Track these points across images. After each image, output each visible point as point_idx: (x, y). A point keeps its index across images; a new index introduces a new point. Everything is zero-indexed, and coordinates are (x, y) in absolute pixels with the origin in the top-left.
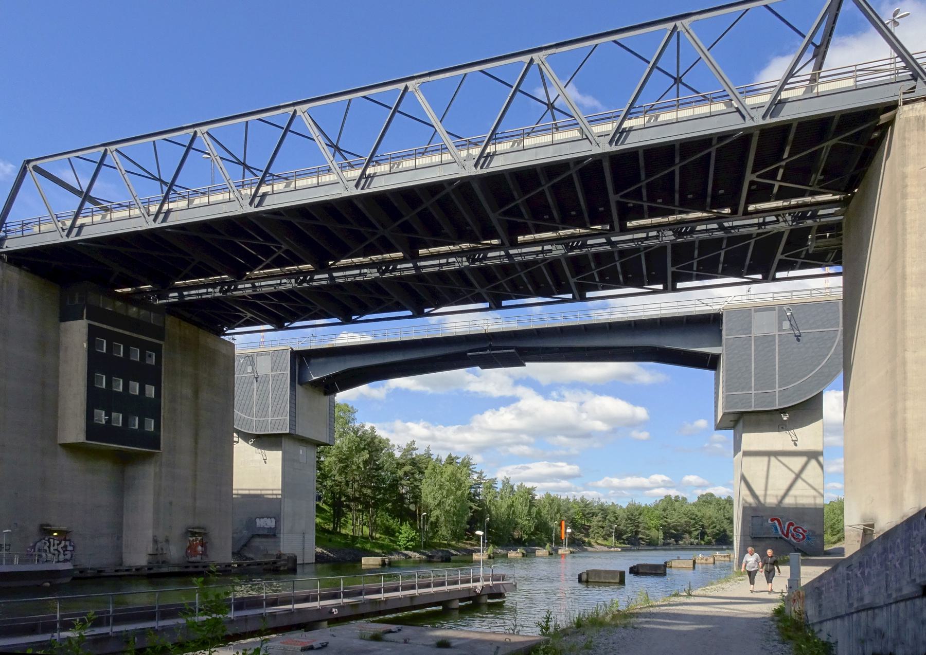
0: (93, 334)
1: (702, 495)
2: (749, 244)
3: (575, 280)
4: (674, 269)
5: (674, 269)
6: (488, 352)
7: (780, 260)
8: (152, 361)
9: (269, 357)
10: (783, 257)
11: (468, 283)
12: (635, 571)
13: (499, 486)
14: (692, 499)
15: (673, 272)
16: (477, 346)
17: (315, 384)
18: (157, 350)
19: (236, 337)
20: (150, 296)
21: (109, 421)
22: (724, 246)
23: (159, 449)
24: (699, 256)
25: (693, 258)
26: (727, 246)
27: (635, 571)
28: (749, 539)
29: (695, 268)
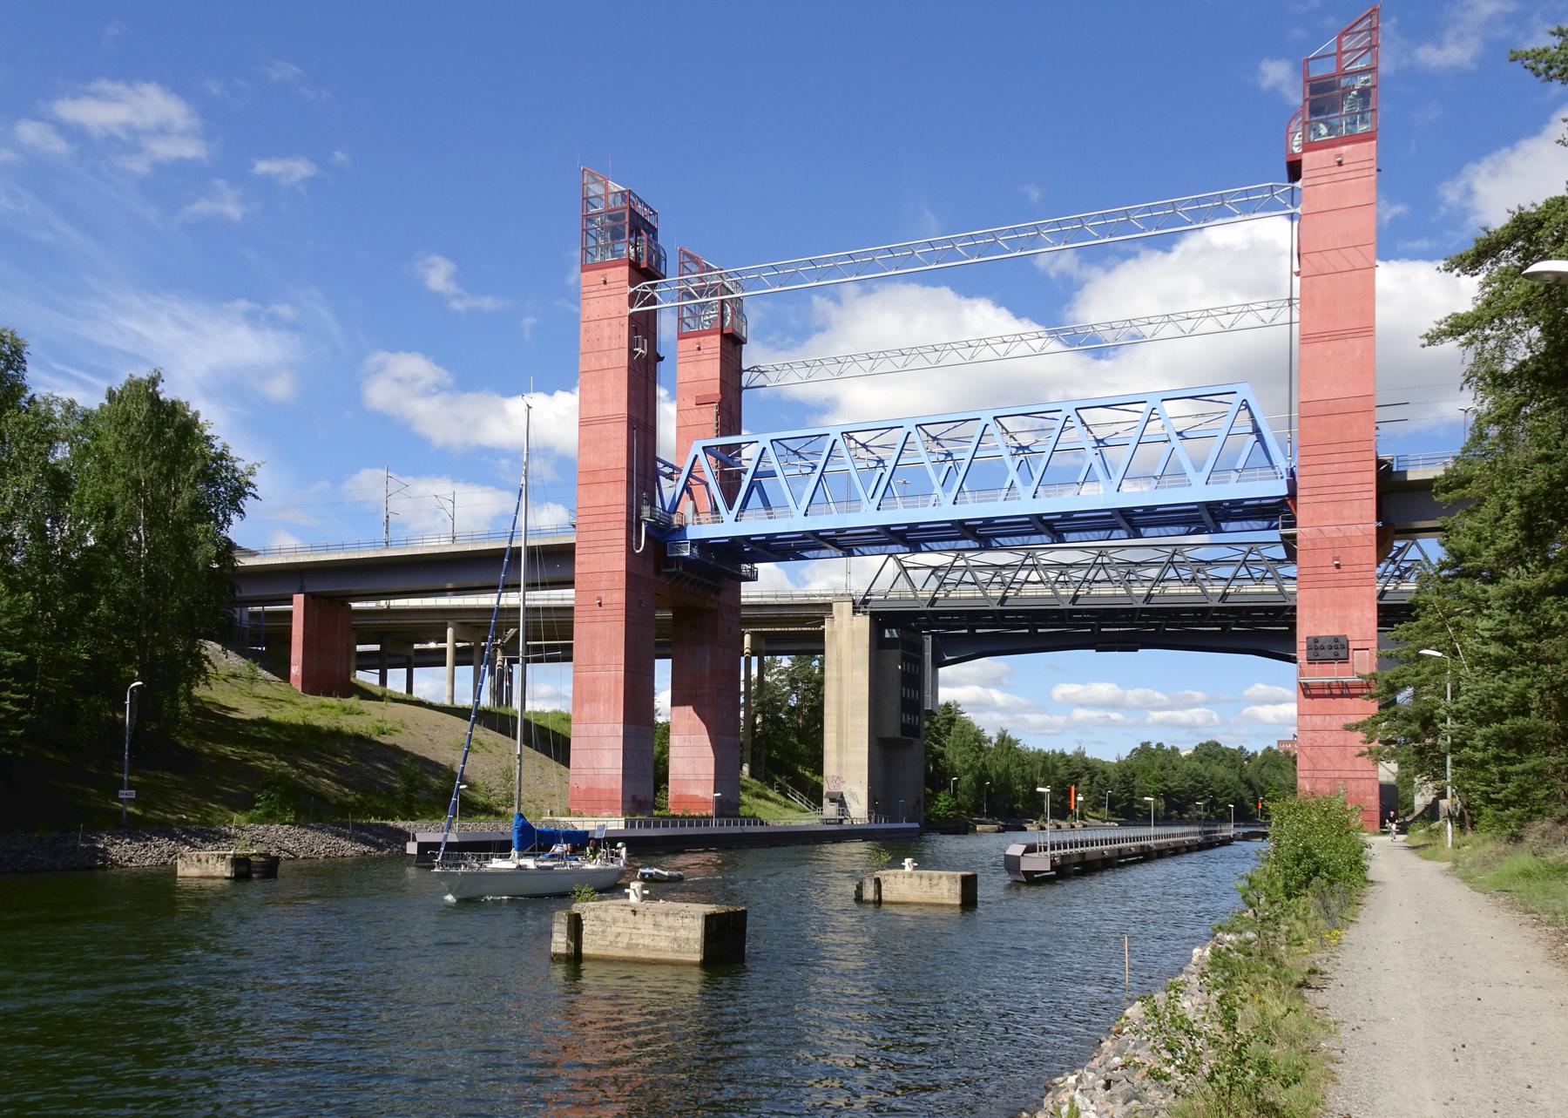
14: (1186, 751)
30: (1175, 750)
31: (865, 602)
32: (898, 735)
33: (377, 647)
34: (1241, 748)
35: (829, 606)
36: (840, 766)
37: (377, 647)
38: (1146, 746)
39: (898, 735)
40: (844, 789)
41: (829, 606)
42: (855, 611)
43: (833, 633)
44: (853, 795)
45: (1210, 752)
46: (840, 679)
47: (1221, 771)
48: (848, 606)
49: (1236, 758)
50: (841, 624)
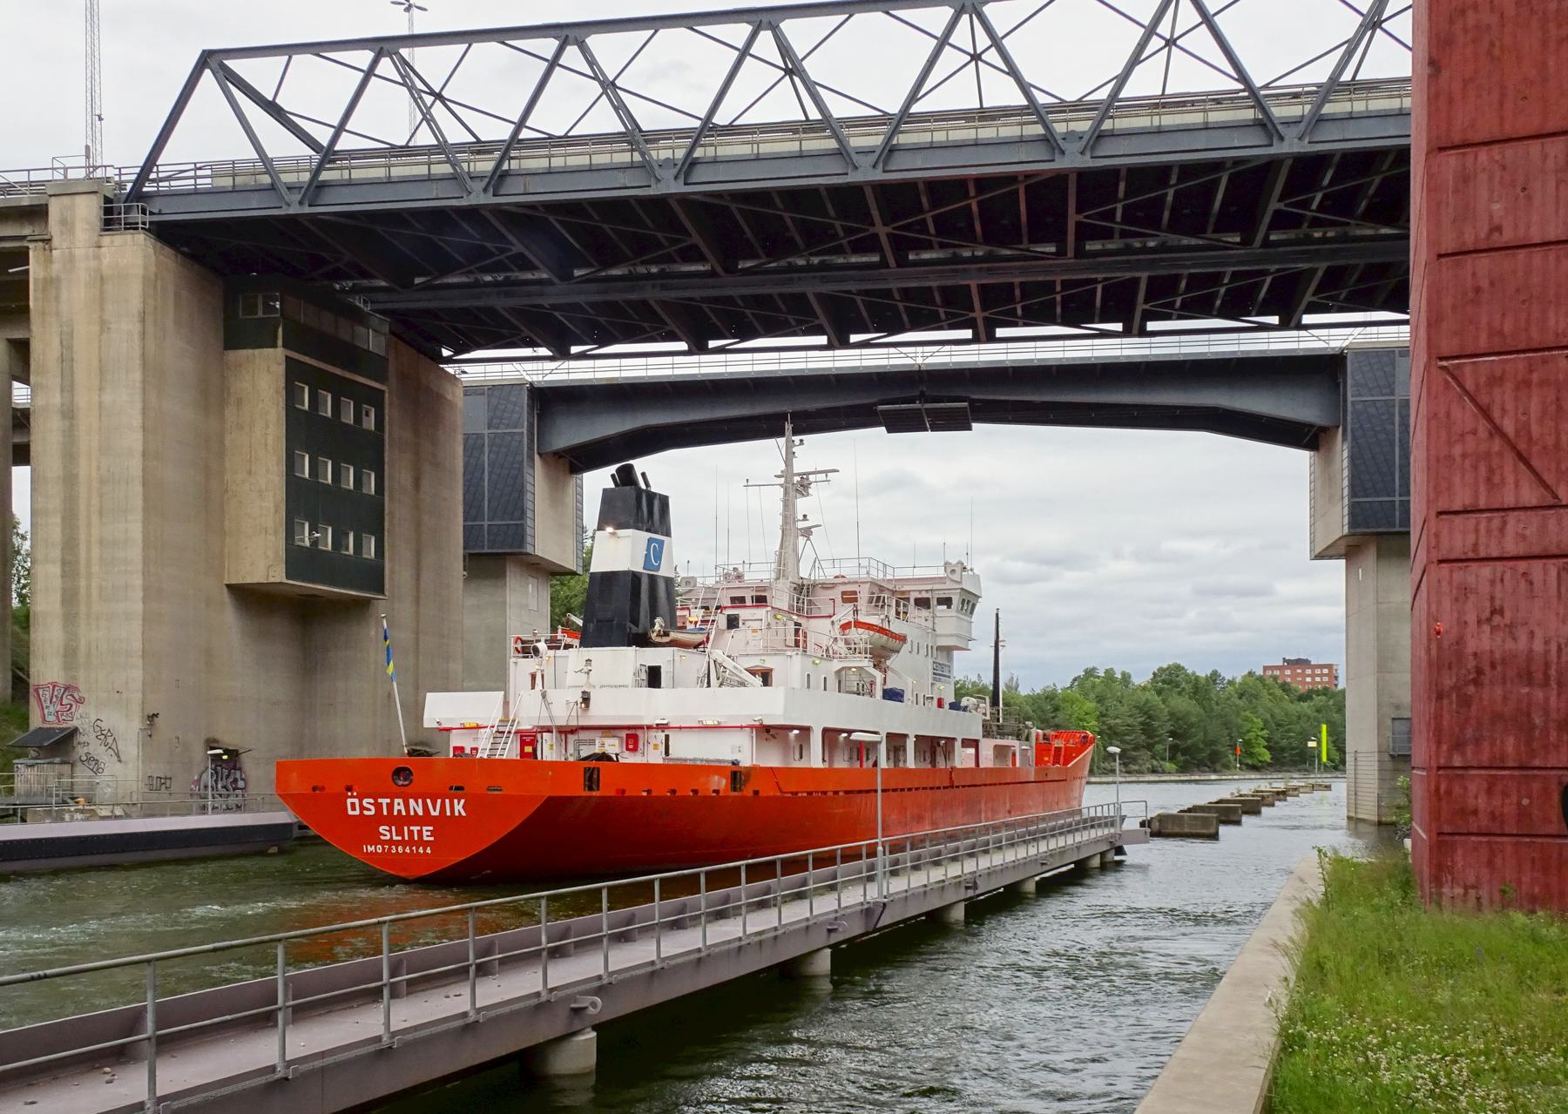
0: (294, 373)
1: (1161, 670)
2: (1216, 182)
3: (889, 229)
4: (1080, 218)
5: (1080, 218)
6: (917, 405)
7: (1277, 213)
8: (370, 423)
9: (484, 399)
10: (1281, 206)
11: (675, 226)
12: (1161, 828)
13: (1119, 676)
14: (1141, 678)
15: (1078, 224)
16: (897, 394)
17: (559, 455)
18: (376, 399)
19: (465, 367)
20: (332, 286)
21: (315, 542)
22: (1173, 182)
23: (383, 593)
24: (1127, 195)
25: (1117, 200)
26: (1180, 180)
27: (1161, 828)
28: (1387, 758)
29: (1118, 218)
30: (1126, 678)
31: (137, 195)
32: (278, 575)
33: (1324, 727)
34: (1215, 673)
35: (37, 213)
36: (70, 655)
37: (1324, 727)
38: (1090, 673)
39: (278, 575)
40: (82, 718)
41: (37, 213)
42: (111, 219)
43: (51, 283)
44: (105, 736)
45: (1170, 679)
46: (69, 413)
47: (1182, 704)
48: (87, 210)
49: (1201, 689)
50: (71, 259)
